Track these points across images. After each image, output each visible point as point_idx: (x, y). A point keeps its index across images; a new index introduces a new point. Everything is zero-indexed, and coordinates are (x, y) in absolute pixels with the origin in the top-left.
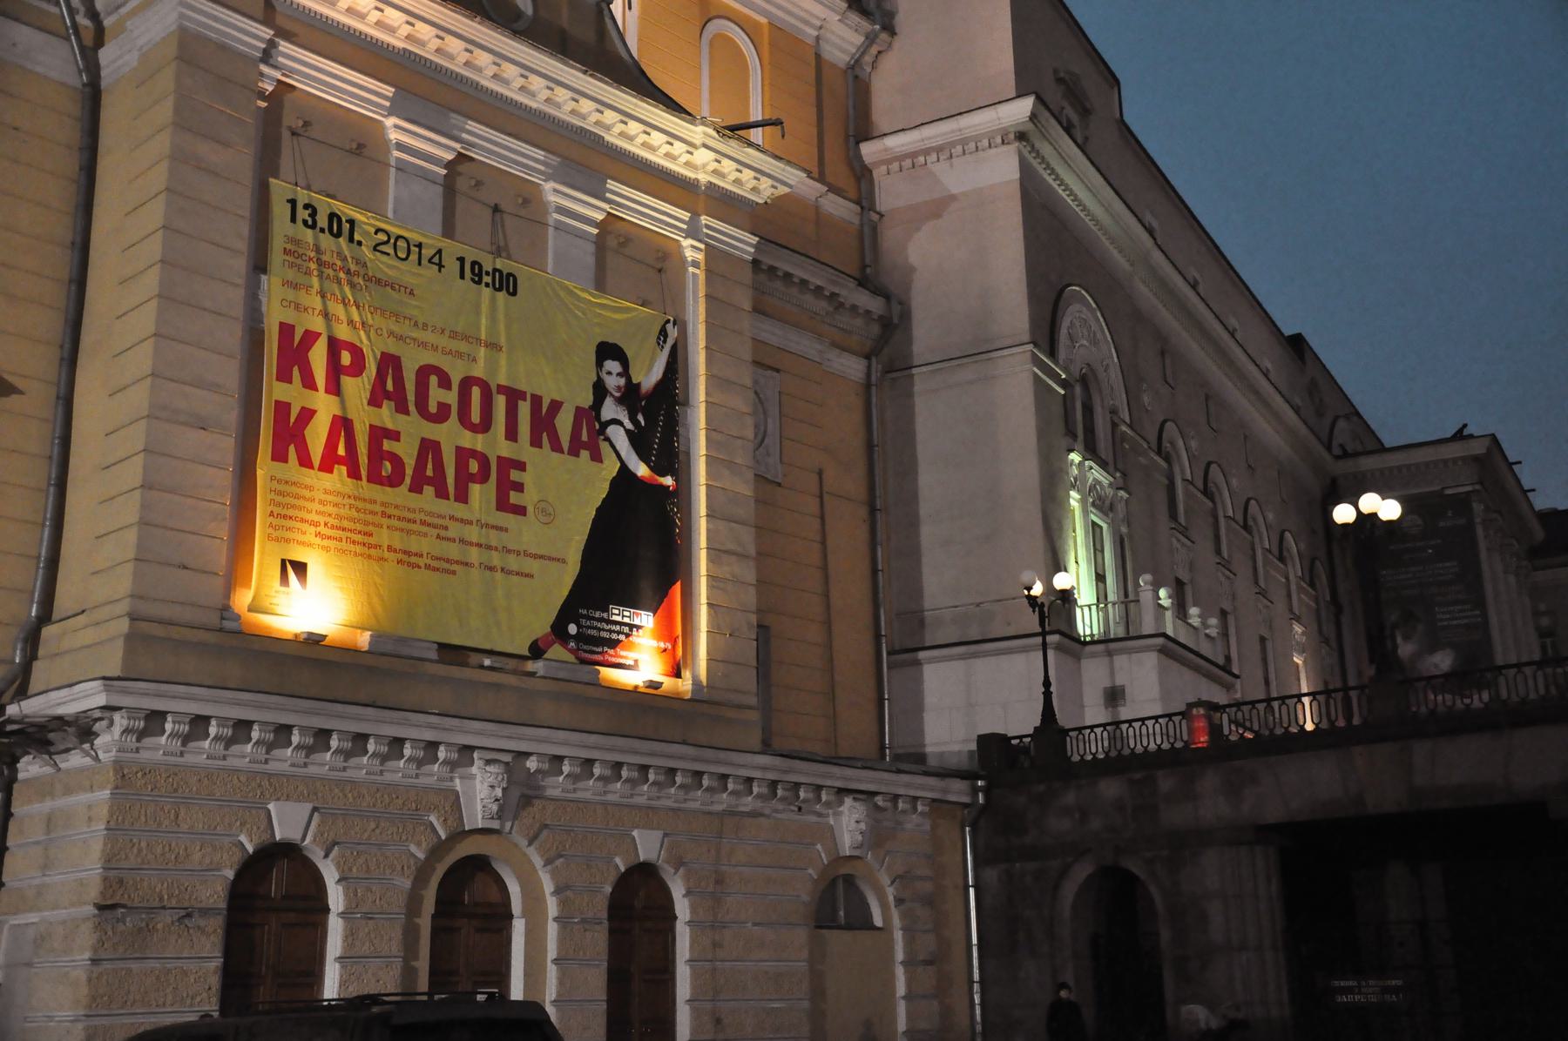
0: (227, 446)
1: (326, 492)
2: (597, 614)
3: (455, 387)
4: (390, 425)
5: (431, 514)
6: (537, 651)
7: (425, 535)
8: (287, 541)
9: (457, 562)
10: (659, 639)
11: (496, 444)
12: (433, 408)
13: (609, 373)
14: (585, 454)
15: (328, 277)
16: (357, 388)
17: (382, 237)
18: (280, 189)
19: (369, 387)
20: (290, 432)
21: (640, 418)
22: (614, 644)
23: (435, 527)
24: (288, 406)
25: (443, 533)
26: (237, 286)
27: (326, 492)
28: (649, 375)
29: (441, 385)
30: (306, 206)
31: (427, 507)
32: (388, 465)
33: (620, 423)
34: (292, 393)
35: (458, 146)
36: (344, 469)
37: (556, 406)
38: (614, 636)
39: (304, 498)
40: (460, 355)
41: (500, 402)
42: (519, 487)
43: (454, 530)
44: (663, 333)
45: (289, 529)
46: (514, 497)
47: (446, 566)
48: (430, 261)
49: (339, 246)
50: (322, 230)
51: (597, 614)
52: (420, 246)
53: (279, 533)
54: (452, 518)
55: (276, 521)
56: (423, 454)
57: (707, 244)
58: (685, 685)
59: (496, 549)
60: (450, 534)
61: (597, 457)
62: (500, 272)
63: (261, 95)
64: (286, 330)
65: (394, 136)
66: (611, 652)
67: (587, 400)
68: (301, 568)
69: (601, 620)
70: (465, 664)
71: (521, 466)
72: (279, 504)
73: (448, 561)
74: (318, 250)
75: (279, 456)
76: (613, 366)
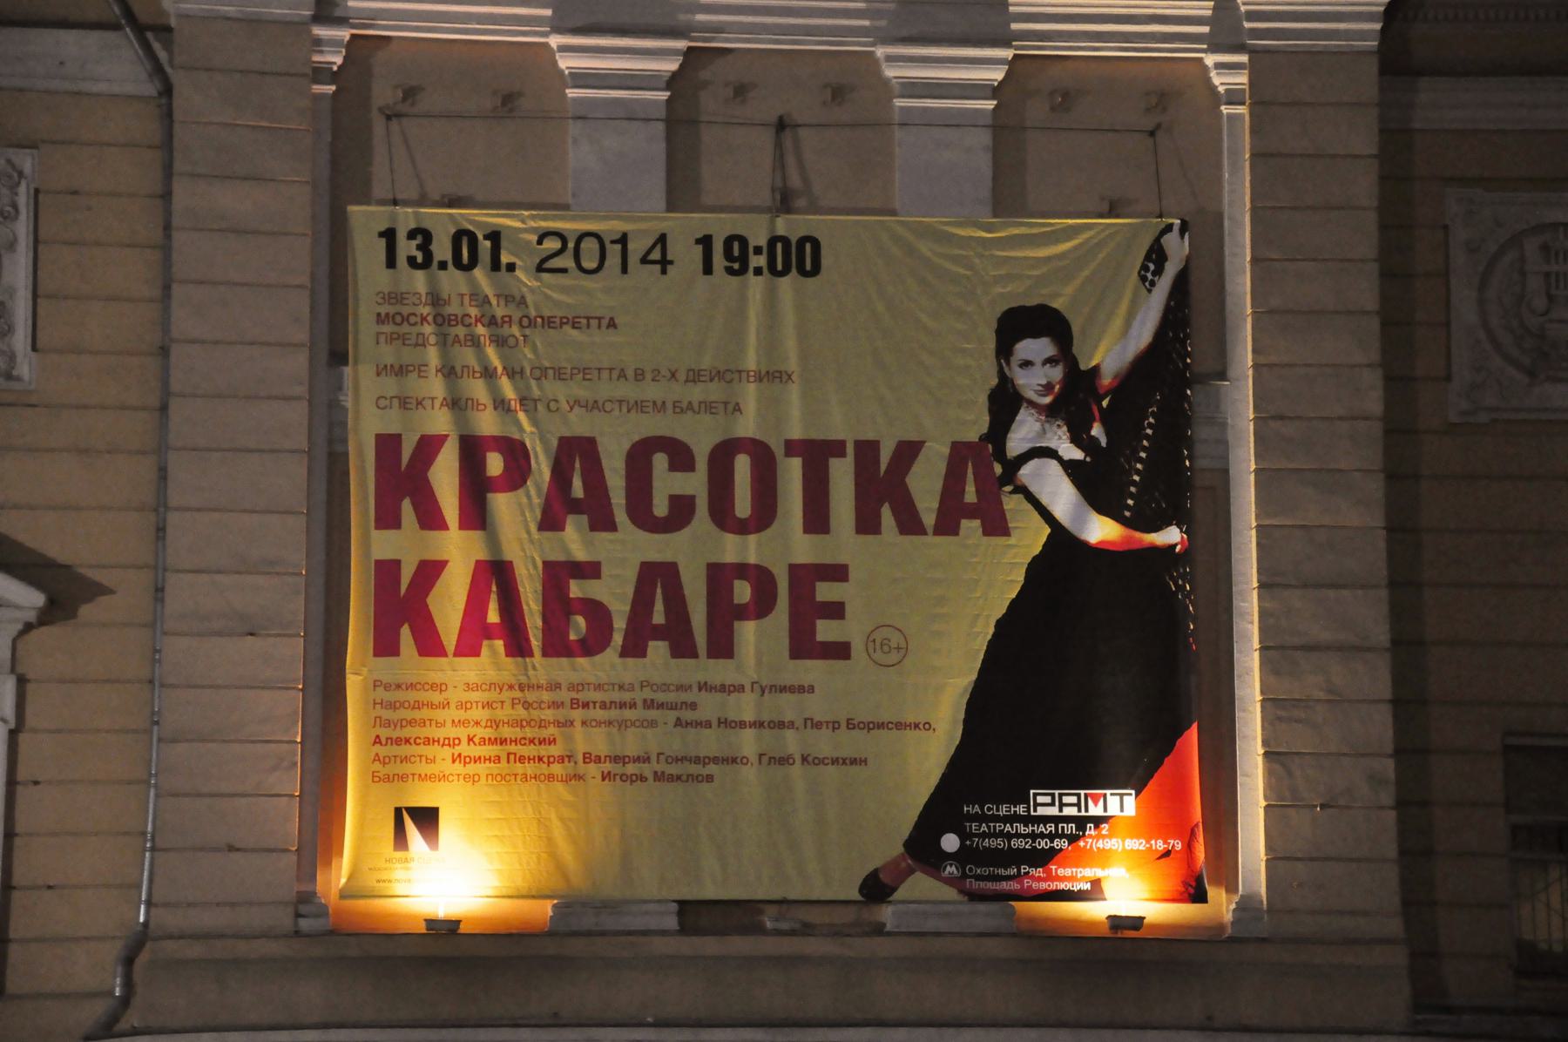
0: (290, 654)
1: (469, 687)
2: (1003, 810)
3: (702, 464)
4: (580, 554)
5: (665, 687)
6: (876, 889)
7: (653, 724)
8: (403, 778)
9: (715, 760)
10: (1162, 831)
11: (788, 544)
12: (661, 508)
13: (1026, 364)
14: (971, 526)
15: (457, 340)
16: (512, 511)
17: (552, 244)
18: (365, 219)
19: (537, 501)
20: (403, 609)
21: (1097, 431)
22: (1044, 858)
23: (673, 707)
24: (395, 565)
25: (688, 715)
26: (298, 398)
27: (469, 687)
28: (1111, 351)
29: (673, 467)
30: (412, 235)
31: (657, 678)
32: (580, 621)
33: (1051, 453)
34: (403, 545)
35: (682, 44)
36: (499, 644)
37: (908, 451)
38: (1043, 844)
39: (431, 705)
40: (708, 407)
41: (792, 472)
42: (836, 611)
43: (709, 707)
44: (1157, 255)
45: (405, 759)
46: (826, 630)
47: (694, 769)
48: (645, 260)
49: (473, 283)
50: (443, 266)
51: (1003, 810)
52: (623, 240)
53: (391, 769)
54: (704, 687)
55: (383, 751)
56: (663, 582)
57: (1252, 51)
58: (1221, 905)
59: (792, 725)
60: (703, 713)
61: (997, 526)
62: (785, 241)
63: (321, 74)
64: (388, 445)
65: (565, 63)
66: (1039, 872)
67: (976, 424)
68: (427, 819)
69: (1015, 818)
70: (759, 930)
71: (838, 573)
72: (388, 724)
73: (697, 760)
74: (436, 300)
75: (386, 646)
76: (1035, 348)
